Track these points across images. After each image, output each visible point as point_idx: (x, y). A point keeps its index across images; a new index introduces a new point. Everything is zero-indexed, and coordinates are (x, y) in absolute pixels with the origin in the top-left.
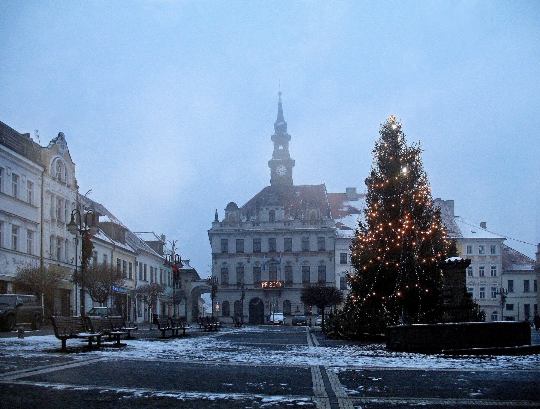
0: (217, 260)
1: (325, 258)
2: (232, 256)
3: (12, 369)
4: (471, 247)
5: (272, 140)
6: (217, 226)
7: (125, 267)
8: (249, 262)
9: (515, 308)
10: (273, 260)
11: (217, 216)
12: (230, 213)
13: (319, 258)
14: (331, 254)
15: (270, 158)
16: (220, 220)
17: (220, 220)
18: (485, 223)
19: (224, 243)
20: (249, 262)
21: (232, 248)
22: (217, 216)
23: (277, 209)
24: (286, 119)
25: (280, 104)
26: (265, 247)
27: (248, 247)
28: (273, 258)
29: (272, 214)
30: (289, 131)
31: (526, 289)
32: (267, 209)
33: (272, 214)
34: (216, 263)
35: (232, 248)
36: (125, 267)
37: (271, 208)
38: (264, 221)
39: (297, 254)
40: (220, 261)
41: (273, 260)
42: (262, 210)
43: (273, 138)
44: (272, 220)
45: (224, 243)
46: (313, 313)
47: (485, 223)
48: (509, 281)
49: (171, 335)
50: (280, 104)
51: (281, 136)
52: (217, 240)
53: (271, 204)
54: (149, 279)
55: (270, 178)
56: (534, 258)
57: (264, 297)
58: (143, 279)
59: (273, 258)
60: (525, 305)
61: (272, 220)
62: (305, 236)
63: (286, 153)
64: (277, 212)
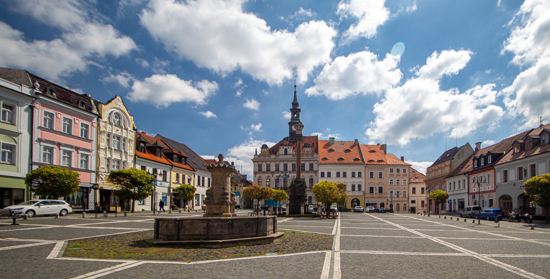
1: (313, 174)
2: (264, 173)
3: (115, 212)
6: (256, 157)
9: (416, 202)
11: (256, 152)
13: (310, 174)
14: (316, 172)
16: (258, 154)
17: (258, 154)
19: (260, 166)
21: (264, 168)
22: (256, 152)
24: (298, 101)
25: (295, 92)
26: (281, 168)
27: (273, 168)
29: (286, 150)
31: (423, 193)
33: (286, 150)
35: (264, 168)
37: (285, 147)
39: (273, 173)
40: (257, 176)
41: (286, 175)
45: (260, 166)
49: (34, 161)
50: (295, 92)
52: (257, 164)
53: (285, 146)
54: (181, 182)
56: (425, 174)
58: (201, 185)
62: (277, 163)
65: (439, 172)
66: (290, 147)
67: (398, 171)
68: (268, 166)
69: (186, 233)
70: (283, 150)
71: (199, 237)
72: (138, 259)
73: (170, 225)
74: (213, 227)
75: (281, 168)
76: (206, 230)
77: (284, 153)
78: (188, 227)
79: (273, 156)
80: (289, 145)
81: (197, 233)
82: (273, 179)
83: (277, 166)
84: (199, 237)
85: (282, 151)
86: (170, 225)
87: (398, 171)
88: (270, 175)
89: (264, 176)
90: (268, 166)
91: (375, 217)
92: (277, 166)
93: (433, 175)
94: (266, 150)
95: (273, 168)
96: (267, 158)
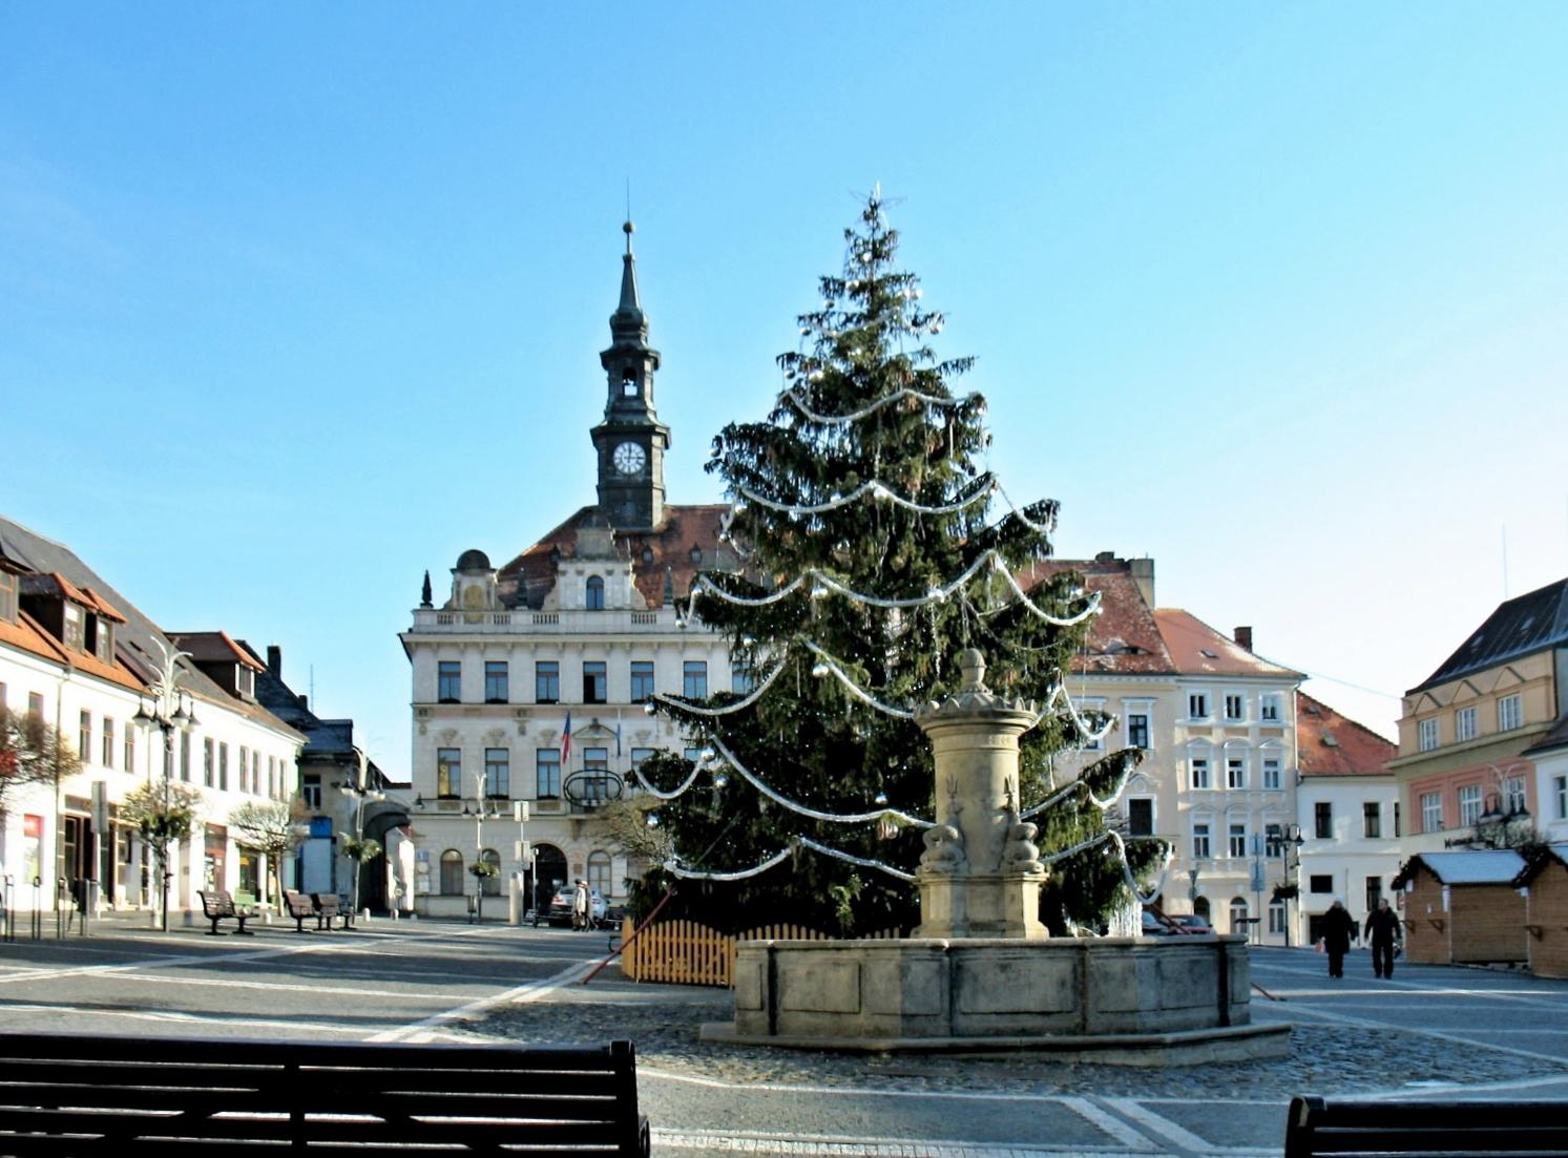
0: (527, 725)
2: (472, 711)
4: (1238, 700)
5: (605, 365)
6: (429, 620)
7: (84, 737)
8: (522, 732)
10: (596, 727)
12: (466, 583)
15: (599, 420)
17: (440, 599)
18: (1249, 629)
19: (449, 673)
20: (522, 732)
21: (473, 687)
23: (610, 573)
24: (643, 302)
27: (522, 687)
28: (595, 720)
29: (595, 585)
30: (652, 340)
32: (580, 573)
33: (595, 585)
34: (423, 732)
35: (473, 687)
36: (84, 737)
37: (592, 568)
38: (618, 605)
39: (521, 712)
40: (436, 726)
41: (596, 727)
42: (564, 573)
43: (608, 359)
44: (595, 604)
45: (449, 673)
46: (61, 902)
47: (1249, 629)
48: (1134, 804)
50: (628, 260)
51: (627, 358)
52: (429, 661)
53: (591, 558)
55: (596, 482)
57: (569, 840)
59: (595, 720)
60: (1369, 879)
61: (595, 604)
63: (638, 405)
64: (608, 582)
65: (1486, 720)
66: (618, 568)
67: (1235, 707)
68: (496, 673)
69: (983, 1004)
70: (582, 583)
71: (1038, 1022)
72: (1063, 1105)
73: (916, 968)
74: (1106, 976)
75: (571, 689)
76: (1069, 993)
77: (582, 600)
78: (991, 976)
79: (522, 618)
80: (608, 558)
81: (1032, 1006)
82: (522, 752)
83: (547, 673)
84: (1038, 1022)
85: (571, 586)
86: (916, 968)
87: (1235, 707)
88: (509, 725)
89: (473, 733)
90: (496, 673)
91: (257, 985)
92: (547, 673)
93: (1443, 731)
94: (480, 582)
95: (522, 687)
96: (488, 626)
